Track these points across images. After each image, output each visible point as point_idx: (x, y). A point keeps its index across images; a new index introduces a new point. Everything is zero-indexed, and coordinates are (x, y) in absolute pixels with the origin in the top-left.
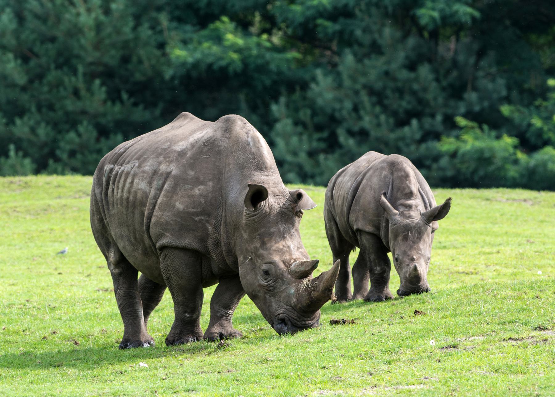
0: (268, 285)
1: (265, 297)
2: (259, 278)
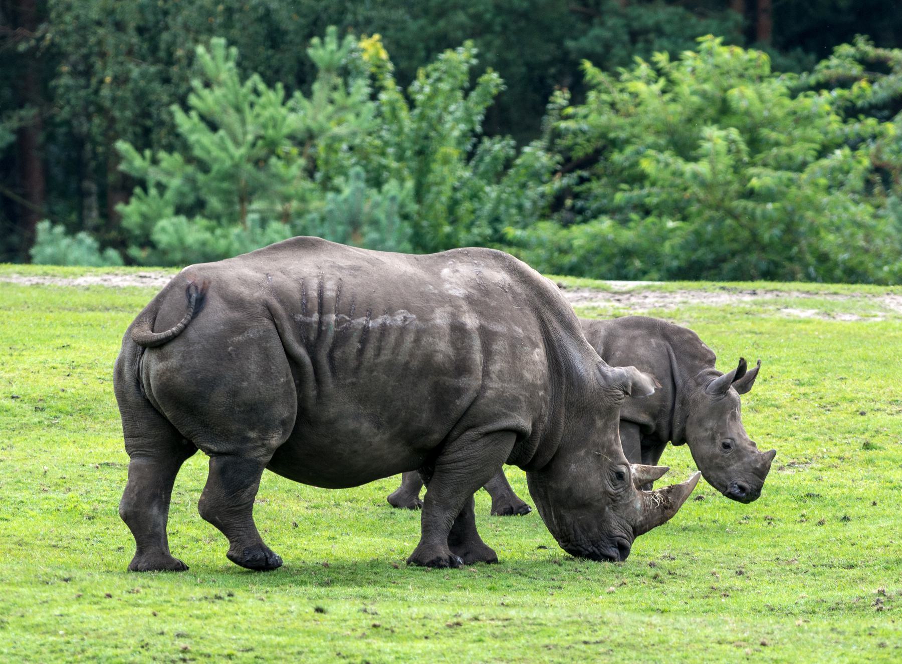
0: (616, 494)
1: (604, 509)
2: (606, 483)
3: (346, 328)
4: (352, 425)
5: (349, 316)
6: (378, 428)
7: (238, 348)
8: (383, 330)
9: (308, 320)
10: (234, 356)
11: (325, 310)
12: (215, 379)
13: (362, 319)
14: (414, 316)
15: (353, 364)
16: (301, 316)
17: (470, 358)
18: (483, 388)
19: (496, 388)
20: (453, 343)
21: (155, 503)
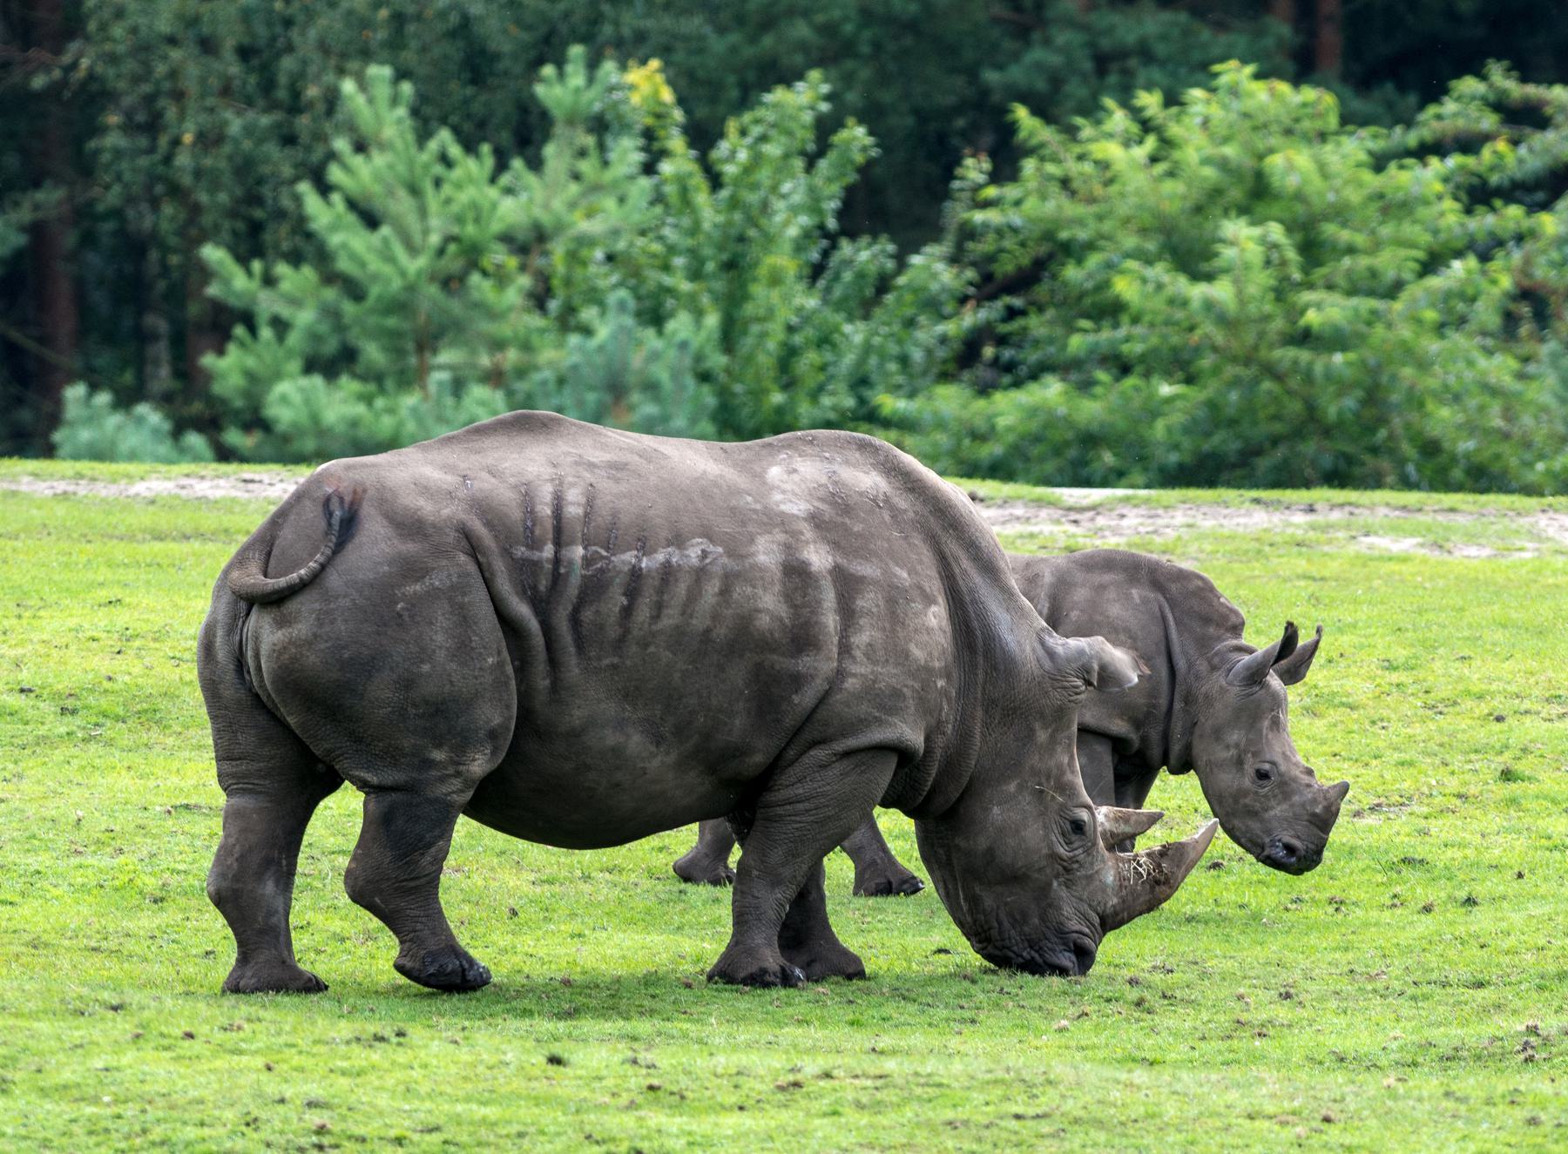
0: (1070, 858)
1: (1050, 885)
2: (1054, 839)
3: (602, 570)
4: (611, 738)
5: (607, 549)
6: (658, 744)
7: (413, 605)
8: (666, 574)
9: (536, 555)
10: (407, 619)
11: (564, 538)
12: (374, 658)
13: (629, 554)
14: (720, 550)
15: (613, 632)
16: (523, 549)
17: (816, 623)
18: (840, 674)
19: (862, 675)
20: (788, 597)
21: (269, 874)
